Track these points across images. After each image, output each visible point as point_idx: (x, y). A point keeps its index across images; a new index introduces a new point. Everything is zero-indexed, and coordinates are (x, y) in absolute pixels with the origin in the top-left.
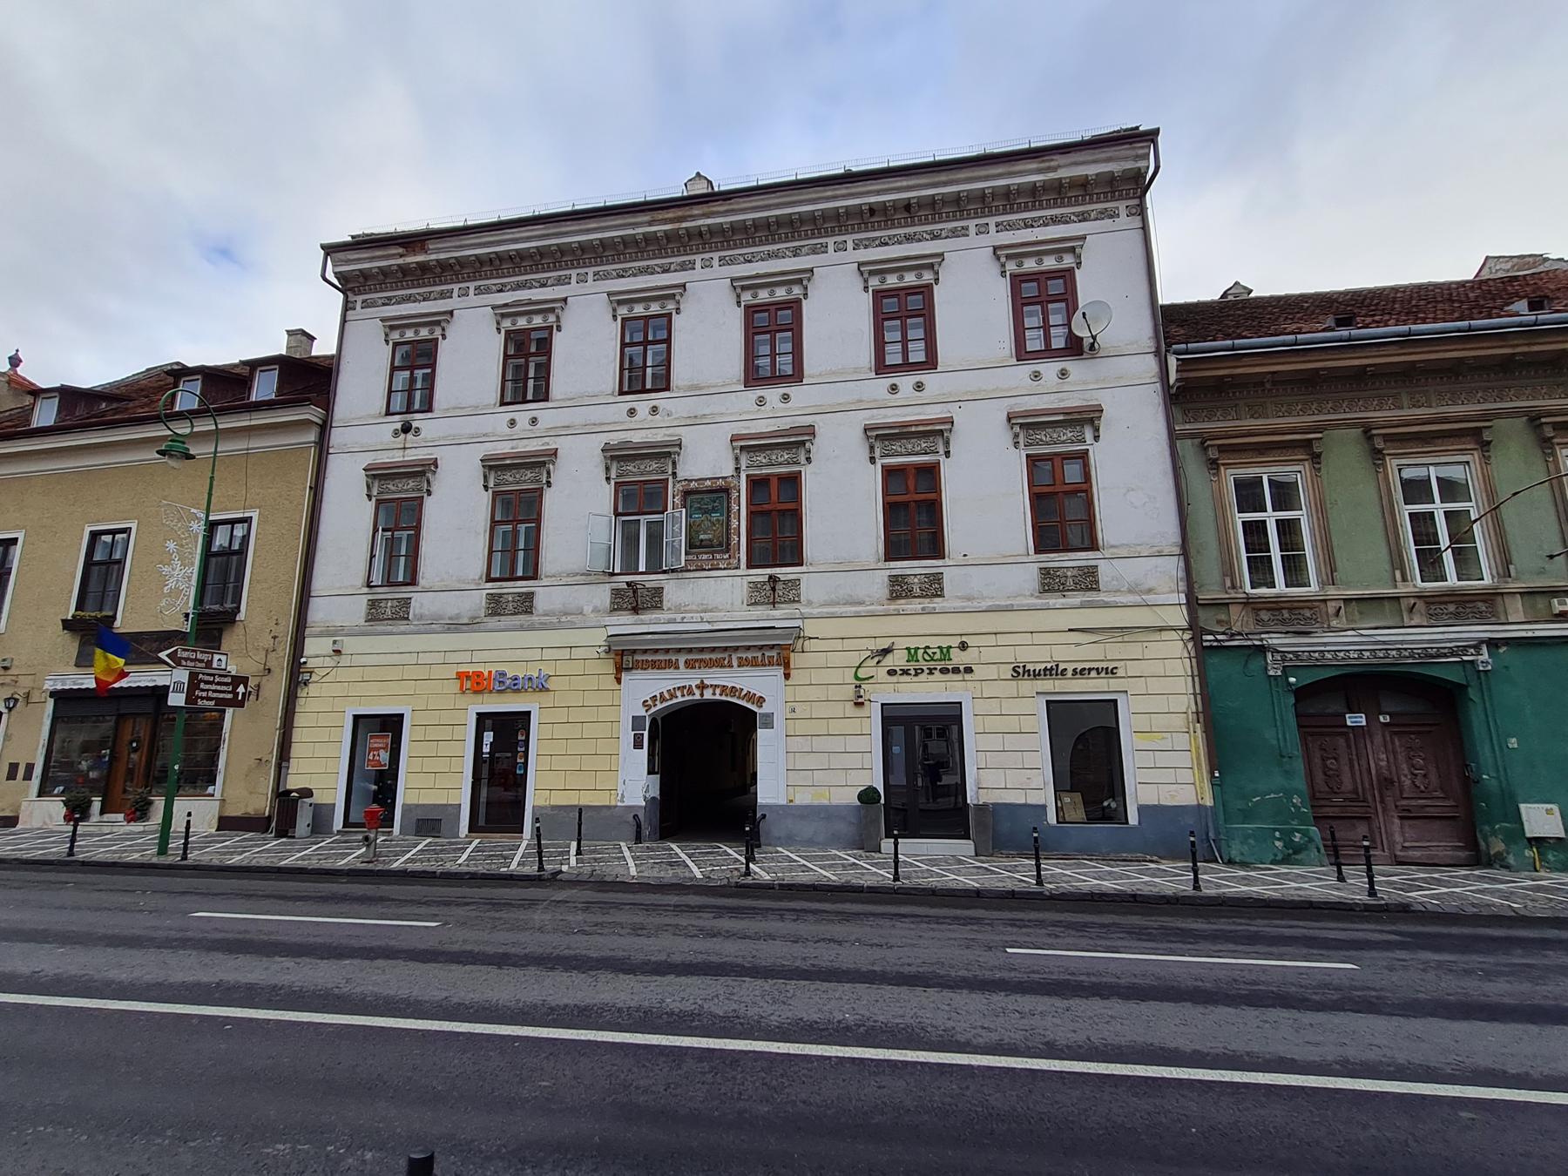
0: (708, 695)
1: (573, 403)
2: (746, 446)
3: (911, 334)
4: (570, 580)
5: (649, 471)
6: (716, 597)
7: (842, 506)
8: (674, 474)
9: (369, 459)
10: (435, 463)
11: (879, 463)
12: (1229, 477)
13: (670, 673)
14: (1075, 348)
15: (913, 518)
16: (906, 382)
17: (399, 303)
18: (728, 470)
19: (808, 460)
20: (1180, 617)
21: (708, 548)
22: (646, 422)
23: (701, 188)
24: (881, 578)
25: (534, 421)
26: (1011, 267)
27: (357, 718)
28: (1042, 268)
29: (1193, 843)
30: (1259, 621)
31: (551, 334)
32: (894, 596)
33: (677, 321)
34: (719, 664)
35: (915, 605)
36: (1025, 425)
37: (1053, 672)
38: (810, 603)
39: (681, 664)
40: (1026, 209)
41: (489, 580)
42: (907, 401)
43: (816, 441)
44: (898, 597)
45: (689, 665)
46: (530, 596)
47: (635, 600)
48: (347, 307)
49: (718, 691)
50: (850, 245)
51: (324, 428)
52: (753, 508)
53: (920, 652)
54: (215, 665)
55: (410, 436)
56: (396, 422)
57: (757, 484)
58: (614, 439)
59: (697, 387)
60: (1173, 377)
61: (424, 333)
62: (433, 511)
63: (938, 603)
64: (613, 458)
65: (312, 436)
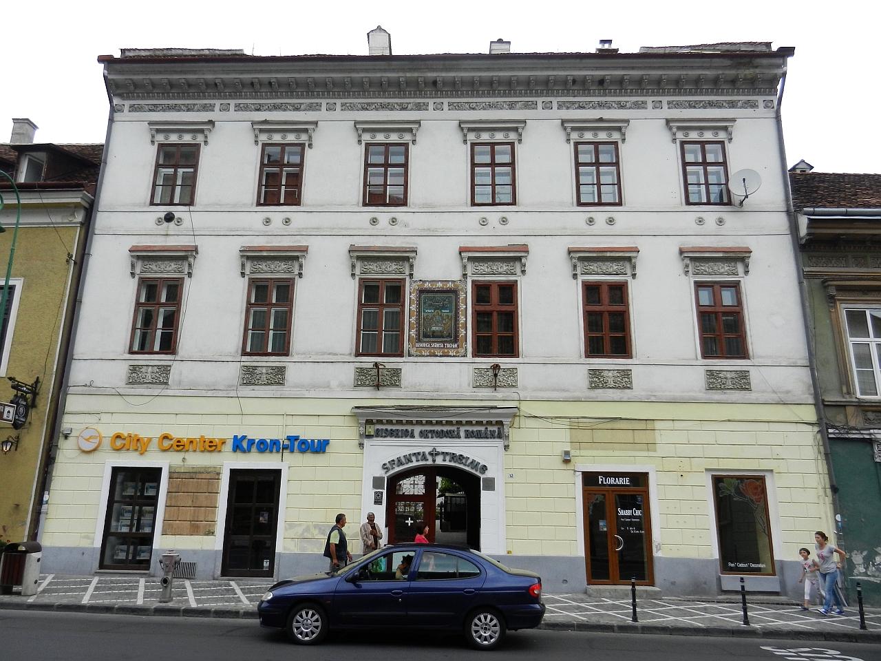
2: (472, 256)
3: (603, 180)
5: (389, 272)
6: (441, 377)
7: (550, 312)
8: (411, 275)
10: (196, 249)
11: (581, 278)
12: (843, 310)
13: (407, 441)
14: (725, 200)
15: (608, 327)
16: (600, 215)
17: (164, 111)
18: (456, 275)
19: (523, 272)
21: (439, 337)
22: (385, 228)
23: (500, 49)
24: (122, 370)
25: (287, 221)
26: (575, 136)
29: (859, 592)
30: (867, 420)
31: (303, 150)
32: (594, 386)
33: (309, 153)
34: (449, 435)
36: (694, 258)
38: (525, 388)
39: (416, 433)
40: (691, 94)
41: (244, 353)
42: (601, 232)
43: (529, 257)
44: (596, 387)
45: (423, 435)
46: (281, 371)
47: (378, 380)
48: (113, 110)
49: (448, 458)
50: (555, 105)
51: (90, 210)
52: (481, 308)
55: (172, 224)
56: (162, 211)
57: (482, 291)
58: (361, 242)
60: (803, 231)
61: (187, 138)
62: (303, 293)
63: (627, 394)
64: (138, 257)
65: (79, 217)
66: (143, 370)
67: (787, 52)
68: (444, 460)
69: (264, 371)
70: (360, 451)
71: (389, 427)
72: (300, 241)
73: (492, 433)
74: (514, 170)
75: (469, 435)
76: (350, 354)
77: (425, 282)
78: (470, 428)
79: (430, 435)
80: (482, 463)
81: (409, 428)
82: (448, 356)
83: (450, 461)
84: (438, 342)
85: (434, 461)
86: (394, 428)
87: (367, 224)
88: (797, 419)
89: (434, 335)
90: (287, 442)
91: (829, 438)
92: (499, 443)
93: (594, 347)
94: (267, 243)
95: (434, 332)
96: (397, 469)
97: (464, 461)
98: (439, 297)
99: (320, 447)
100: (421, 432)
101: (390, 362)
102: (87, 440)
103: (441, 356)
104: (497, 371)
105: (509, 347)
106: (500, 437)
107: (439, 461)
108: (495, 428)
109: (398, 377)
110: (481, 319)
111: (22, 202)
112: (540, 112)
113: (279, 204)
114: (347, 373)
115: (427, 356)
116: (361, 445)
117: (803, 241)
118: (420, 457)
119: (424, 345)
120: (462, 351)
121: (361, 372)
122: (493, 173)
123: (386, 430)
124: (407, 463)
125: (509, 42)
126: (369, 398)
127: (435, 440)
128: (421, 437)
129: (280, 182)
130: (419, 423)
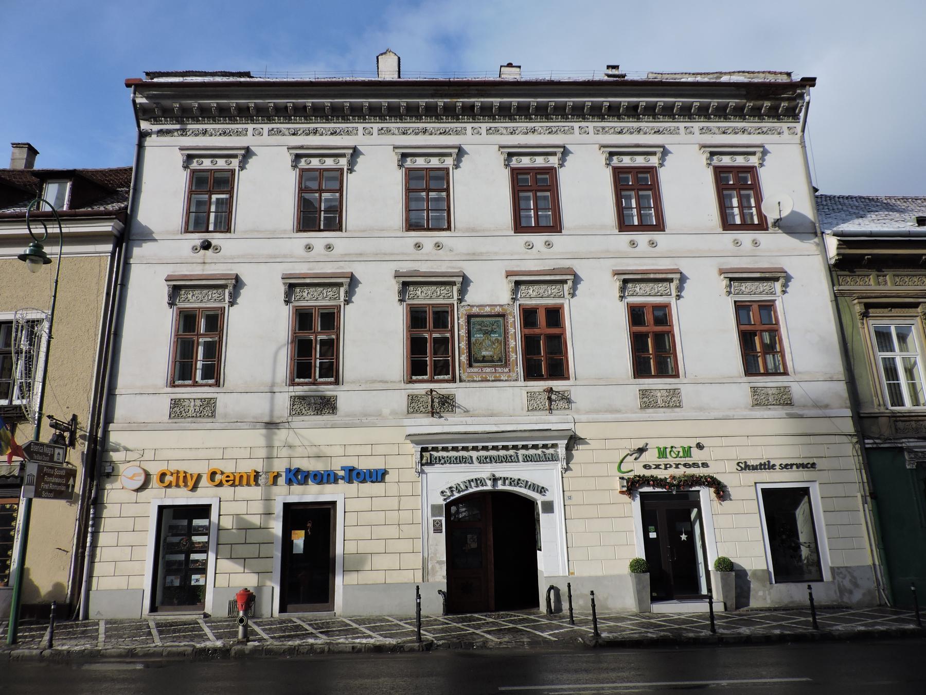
0: (500, 487)
1: (366, 234)
4: (368, 386)
6: (496, 401)
9: (394, 266)
12: (873, 323)
15: (652, 346)
16: (642, 238)
20: (848, 426)
22: (431, 254)
24: (164, 404)
25: (329, 247)
27: (161, 508)
28: (735, 164)
32: (645, 406)
34: (505, 460)
35: (661, 414)
37: (767, 466)
44: (647, 407)
45: (481, 460)
52: (527, 331)
53: (668, 450)
54: (55, 459)
55: (209, 253)
56: (197, 239)
57: (529, 315)
58: (405, 267)
59: (473, 230)
66: (186, 403)
67: (810, 82)
69: (659, 394)
71: (445, 454)
72: (342, 267)
74: (341, 195)
75: (527, 459)
77: (473, 306)
84: (489, 367)
87: (411, 249)
88: (839, 432)
89: (484, 360)
90: (342, 473)
91: (866, 449)
93: (641, 369)
94: (309, 269)
95: (484, 357)
98: (487, 322)
99: (378, 476)
101: (443, 388)
102: (131, 478)
105: (558, 370)
110: (530, 344)
111: (64, 230)
112: (682, 137)
113: (320, 230)
114: (398, 399)
117: (833, 262)
119: (476, 370)
120: (514, 375)
121: (412, 399)
122: (535, 197)
125: (520, 67)
126: (426, 425)
129: (318, 210)
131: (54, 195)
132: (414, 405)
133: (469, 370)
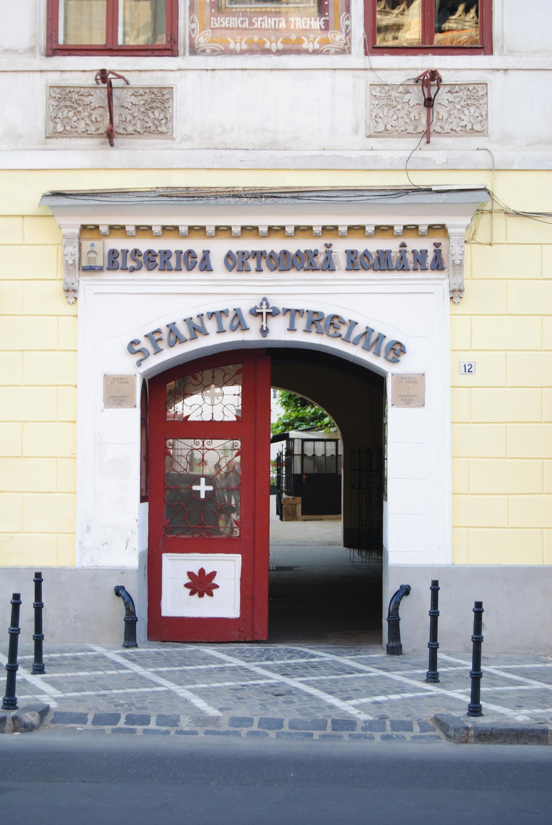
4: (301, 194)
34: (303, 262)
45: (236, 262)
47: (109, 115)
49: (301, 323)
68: (292, 329)
70: (69, 310)
73: (420, 259)
75: (356, 262)
76: (32, 50)
78: (360, 245)
79: (252, 263)
80: (391, 336)
81: (198, 246)
82: (299, 52)
83: (307, 331)
85: (264, 332)
86: (157, 245)
92: (436, 283)
96: (169, 354)
97: (343, 331)
100: (229, 255)
103: (279, 53)
104: (433, 90)
106: (438, 265)
107: (279, 333)
108: (426, 244)
109: (164, 110)
115: (243, 52)
116: (70, 291)
118: (226, 322)
119: (234, 22)
121: (64, 98)
123: (136, 252)
124: (194, 338)
127: (267, 275)
128: (230, 269)
130: (223, 231)
131: (208, 51)
132: (65, 113)
133: (215, 22)
